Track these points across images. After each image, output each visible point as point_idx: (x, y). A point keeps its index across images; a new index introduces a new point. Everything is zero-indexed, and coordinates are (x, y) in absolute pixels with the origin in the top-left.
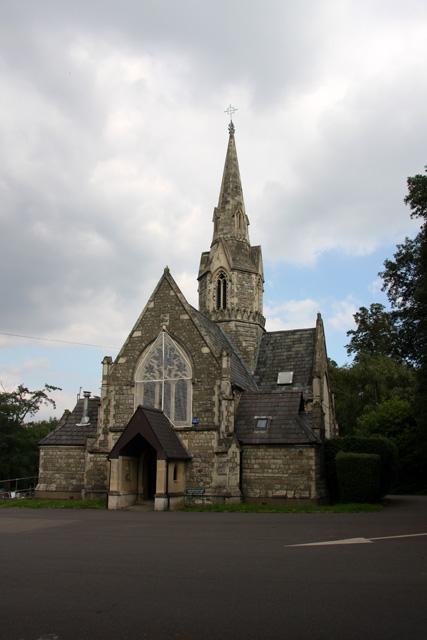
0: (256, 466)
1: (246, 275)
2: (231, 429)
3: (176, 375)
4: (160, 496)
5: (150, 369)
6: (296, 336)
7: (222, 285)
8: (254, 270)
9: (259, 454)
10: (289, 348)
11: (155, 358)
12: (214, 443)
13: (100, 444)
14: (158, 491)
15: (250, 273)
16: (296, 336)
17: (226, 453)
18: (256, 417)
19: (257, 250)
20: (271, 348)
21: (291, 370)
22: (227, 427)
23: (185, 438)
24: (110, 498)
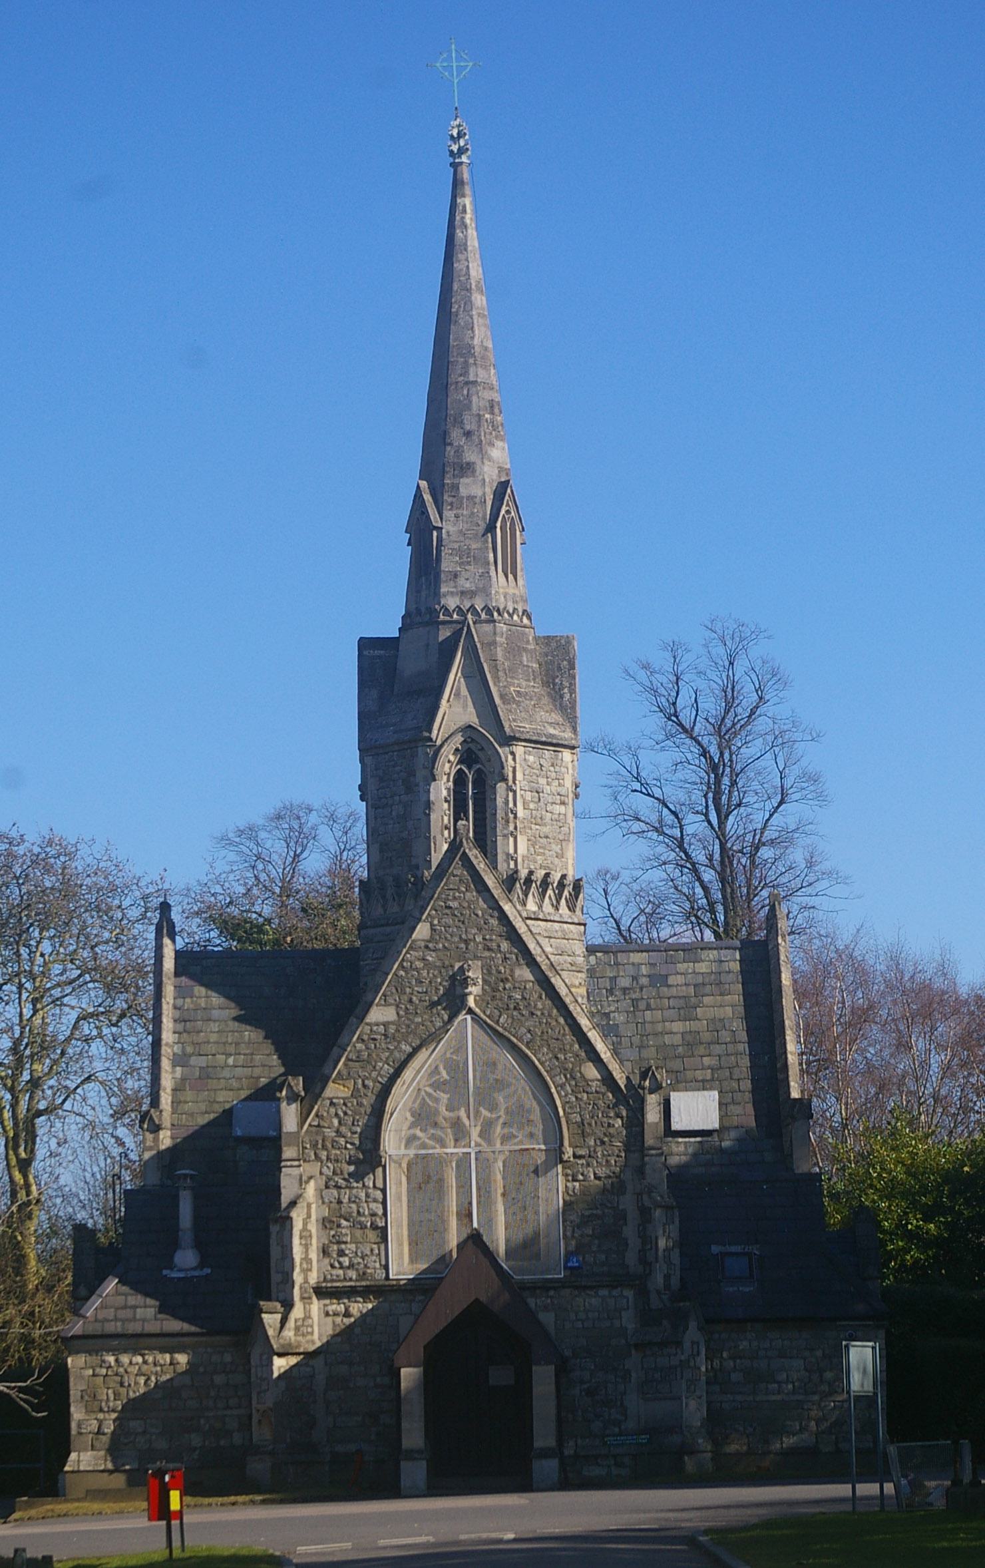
0: (735, 1377)
1: (548, 754)
2: (675, 1282)
3: (505, 1139)
4: (545, 1454)
5: (423, 1116)
6: (702, 967)
7: (729, 896)
8: (567, 735)
9: (744, 1345)
10: (687, 1010)
11: (436, 1086)
12: (628, 1320)
13: (297, 1329)
14: (538, 1443)
15: (558, 745)
16: (702, 967)
17: (679, 1344)
18: (715, 1249)
19: (406, 532)
20: (626, 1004)
21: (704, 1085)
22: (667, 1277)
23: (546, 1308)
24: (404, 1465)
